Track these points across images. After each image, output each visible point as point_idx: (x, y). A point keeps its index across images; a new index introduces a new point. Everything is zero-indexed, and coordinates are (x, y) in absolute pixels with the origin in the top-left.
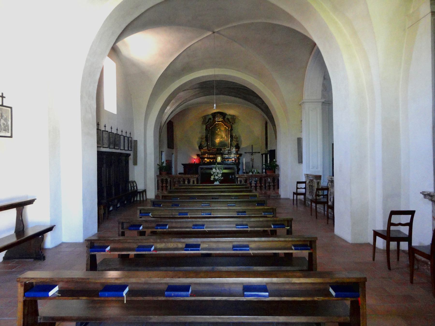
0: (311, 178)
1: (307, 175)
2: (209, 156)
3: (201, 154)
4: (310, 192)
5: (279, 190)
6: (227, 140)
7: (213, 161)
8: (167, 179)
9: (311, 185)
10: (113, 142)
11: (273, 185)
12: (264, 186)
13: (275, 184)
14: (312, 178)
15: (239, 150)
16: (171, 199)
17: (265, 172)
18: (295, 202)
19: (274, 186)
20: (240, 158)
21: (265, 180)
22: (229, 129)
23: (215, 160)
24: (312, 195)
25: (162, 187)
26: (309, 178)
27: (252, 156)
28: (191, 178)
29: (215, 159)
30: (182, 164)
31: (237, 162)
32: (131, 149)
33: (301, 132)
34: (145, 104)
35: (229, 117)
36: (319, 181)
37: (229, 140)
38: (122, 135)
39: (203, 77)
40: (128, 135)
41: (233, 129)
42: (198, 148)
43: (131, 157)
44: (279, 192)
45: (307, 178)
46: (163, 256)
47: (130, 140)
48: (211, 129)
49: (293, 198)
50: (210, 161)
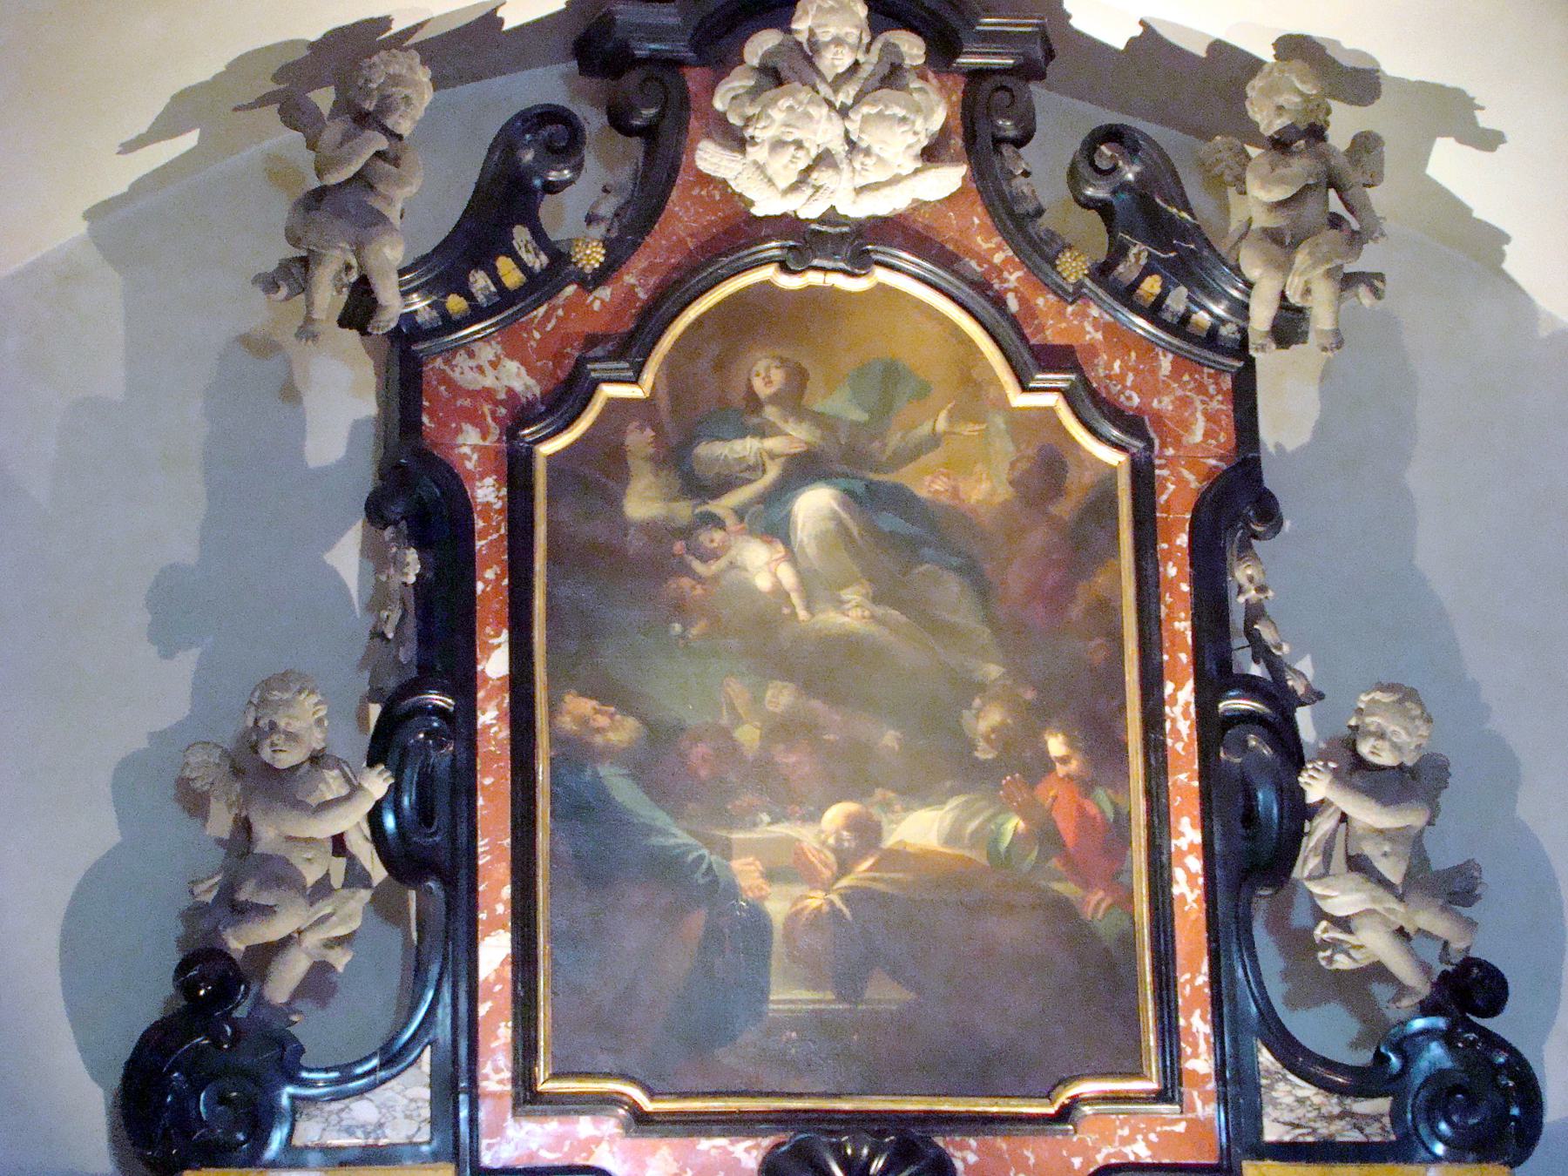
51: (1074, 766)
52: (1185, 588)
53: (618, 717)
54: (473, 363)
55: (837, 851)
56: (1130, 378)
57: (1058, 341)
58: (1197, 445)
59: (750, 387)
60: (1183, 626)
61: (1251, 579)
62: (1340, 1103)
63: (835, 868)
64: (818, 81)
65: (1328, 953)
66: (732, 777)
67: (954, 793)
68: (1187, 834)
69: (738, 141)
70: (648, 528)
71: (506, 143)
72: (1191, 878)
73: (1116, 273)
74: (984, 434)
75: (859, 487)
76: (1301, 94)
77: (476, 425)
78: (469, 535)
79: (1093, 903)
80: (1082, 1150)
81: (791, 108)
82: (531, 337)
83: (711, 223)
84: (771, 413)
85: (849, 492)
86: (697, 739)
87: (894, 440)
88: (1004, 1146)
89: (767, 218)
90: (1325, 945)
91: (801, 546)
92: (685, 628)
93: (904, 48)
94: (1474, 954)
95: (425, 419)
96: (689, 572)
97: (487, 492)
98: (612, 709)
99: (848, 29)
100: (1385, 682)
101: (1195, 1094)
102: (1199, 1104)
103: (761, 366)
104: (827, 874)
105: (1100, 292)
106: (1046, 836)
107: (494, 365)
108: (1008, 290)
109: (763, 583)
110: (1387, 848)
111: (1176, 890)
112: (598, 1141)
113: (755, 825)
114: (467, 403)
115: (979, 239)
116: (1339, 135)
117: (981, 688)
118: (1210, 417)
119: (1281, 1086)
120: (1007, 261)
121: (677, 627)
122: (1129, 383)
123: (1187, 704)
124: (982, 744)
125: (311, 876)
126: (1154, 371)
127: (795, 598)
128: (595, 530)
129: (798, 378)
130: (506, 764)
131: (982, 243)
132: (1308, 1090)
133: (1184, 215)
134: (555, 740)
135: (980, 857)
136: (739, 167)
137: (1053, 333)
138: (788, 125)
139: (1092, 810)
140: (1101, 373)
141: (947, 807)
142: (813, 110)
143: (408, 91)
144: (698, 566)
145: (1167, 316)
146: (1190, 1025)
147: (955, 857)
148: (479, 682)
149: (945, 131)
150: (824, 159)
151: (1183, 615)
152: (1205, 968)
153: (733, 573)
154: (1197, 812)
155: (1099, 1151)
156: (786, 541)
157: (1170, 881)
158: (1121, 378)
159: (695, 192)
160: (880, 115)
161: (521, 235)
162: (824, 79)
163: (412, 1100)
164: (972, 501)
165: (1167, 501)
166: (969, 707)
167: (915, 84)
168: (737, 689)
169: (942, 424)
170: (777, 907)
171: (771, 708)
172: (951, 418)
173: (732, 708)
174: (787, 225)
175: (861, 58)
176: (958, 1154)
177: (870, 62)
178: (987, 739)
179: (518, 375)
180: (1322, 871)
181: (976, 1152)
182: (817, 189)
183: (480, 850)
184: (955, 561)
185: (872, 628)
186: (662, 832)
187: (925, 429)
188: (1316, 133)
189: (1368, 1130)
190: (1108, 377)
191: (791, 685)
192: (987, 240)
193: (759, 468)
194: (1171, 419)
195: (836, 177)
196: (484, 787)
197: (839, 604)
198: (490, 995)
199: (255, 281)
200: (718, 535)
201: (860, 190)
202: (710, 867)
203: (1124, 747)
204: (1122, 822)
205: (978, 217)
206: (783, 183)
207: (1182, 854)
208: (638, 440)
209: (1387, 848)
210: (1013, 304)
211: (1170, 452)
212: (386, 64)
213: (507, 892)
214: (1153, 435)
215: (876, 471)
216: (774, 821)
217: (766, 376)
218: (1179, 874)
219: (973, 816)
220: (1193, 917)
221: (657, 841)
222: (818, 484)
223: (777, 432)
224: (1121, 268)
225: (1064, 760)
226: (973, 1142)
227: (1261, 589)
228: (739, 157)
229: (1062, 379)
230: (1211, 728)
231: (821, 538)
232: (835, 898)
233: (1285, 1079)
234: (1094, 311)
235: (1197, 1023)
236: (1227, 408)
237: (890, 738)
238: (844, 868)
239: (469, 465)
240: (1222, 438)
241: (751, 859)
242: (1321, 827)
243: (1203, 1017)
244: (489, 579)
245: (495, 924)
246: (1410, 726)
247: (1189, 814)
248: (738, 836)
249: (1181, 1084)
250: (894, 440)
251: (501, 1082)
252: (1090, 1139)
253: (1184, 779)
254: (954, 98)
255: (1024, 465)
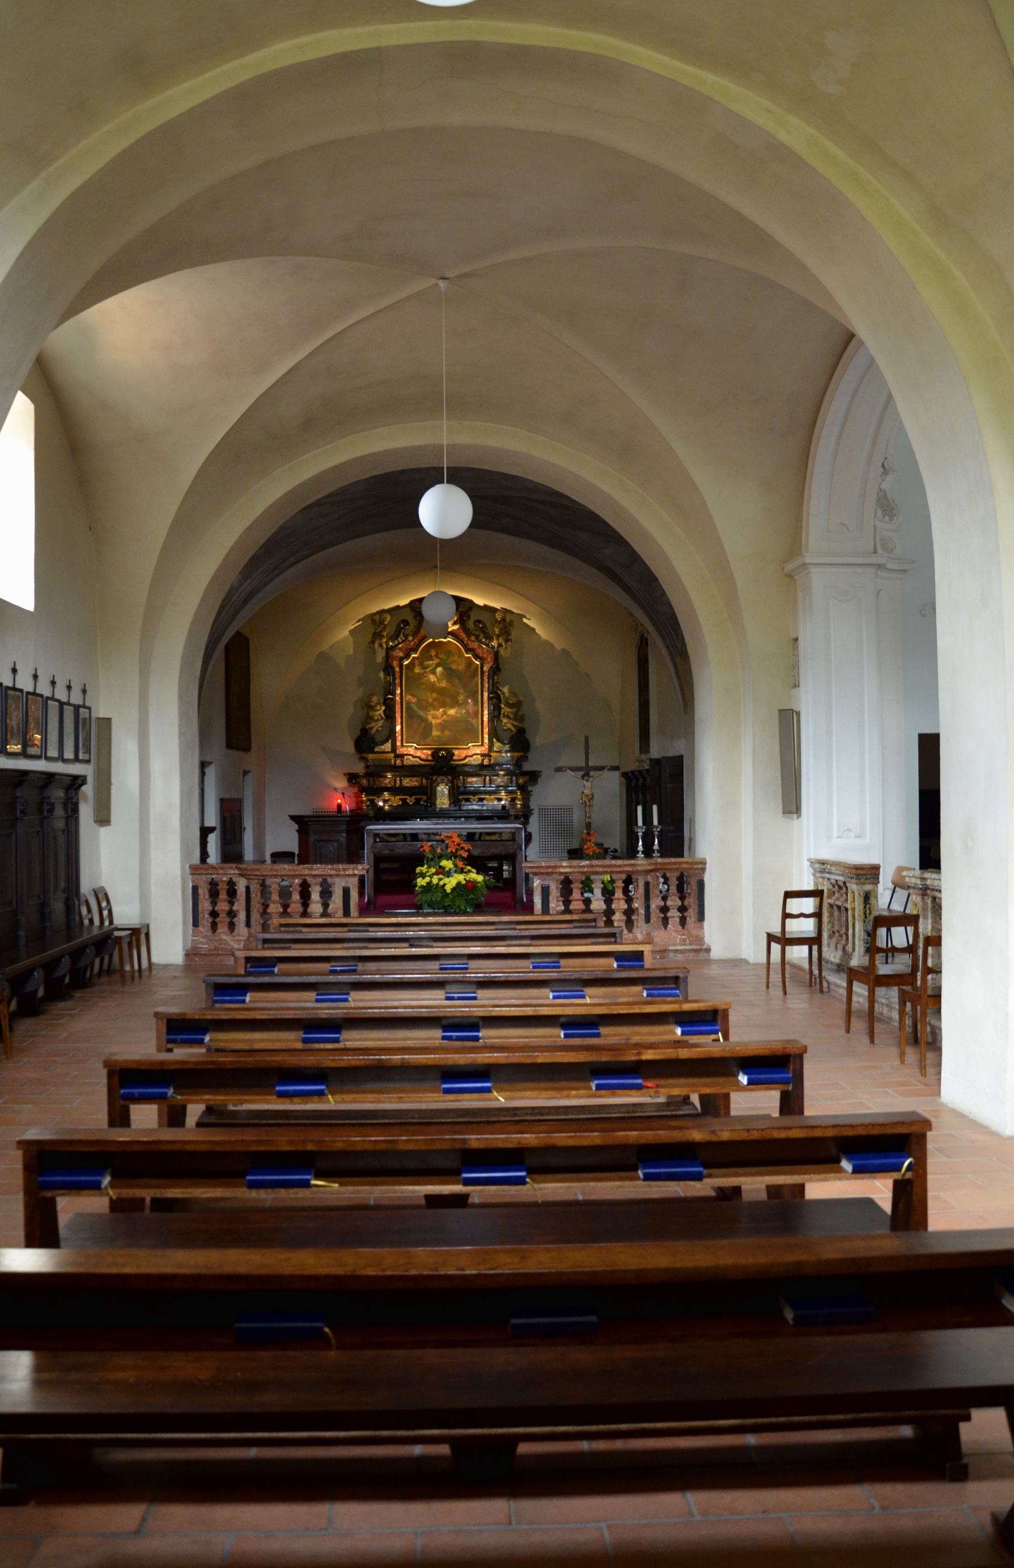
0: (839, 875)
1: (823, 863)
2: (398, 782)
3: (367, 775)
4: (834, 932)
5: (702, 928)
6: (476, 713)
7: (418, 801)
8: (234, 880)
9: (839, 903)
10: (18, 729)
11: (626, 910)
12: (642, 911)
13: (217, 908)
14: (841, 878)
15: (525, 758)
16: (830, 937)
17: (643, 852)
18: (776, 977)
19: (682, 909)
20: (530, 788)
21: (647, 885)
22: (485, 668)
23: (425, 798)
24: (840, 947)
25: (214, 914)
26: (827, 875)
27: (585, 783)
28: (337, 876)
29: (425, 794)
30: (293, 818)
31: (519, 806)
32: (86, 757)
33: (796, 685)
34: (149, 563)
35: (484, 617)
36: (868, 887)
37: (486, 712)
38: (53, 699)
39: (394, 452)
40: (76, 698)
41: (501, 666)
42: (350, 747)
43: (88, 789)
44: (703, 934)
45: (818, 875)
46: (268, 1205)
47: (81, 716)
48: (406, 665)
49: (764, 960)
50: (404, 801)
71: (399, 625)
84: (434, 658)
97: (397, 669)
106: (467, 712)
116: (508, 620)
129: (437, 653)
131: (462, 634)
134: (406, 701)
168: (429, 694)
169: (456, 658)
170: (434, 722)
193: (432, 665)
204: (478, 710)
205: (461, 631)
208: (417, 662)
217: (433, 653)
235: (486, 736)
237: (448, 700)
238: (442, 717)
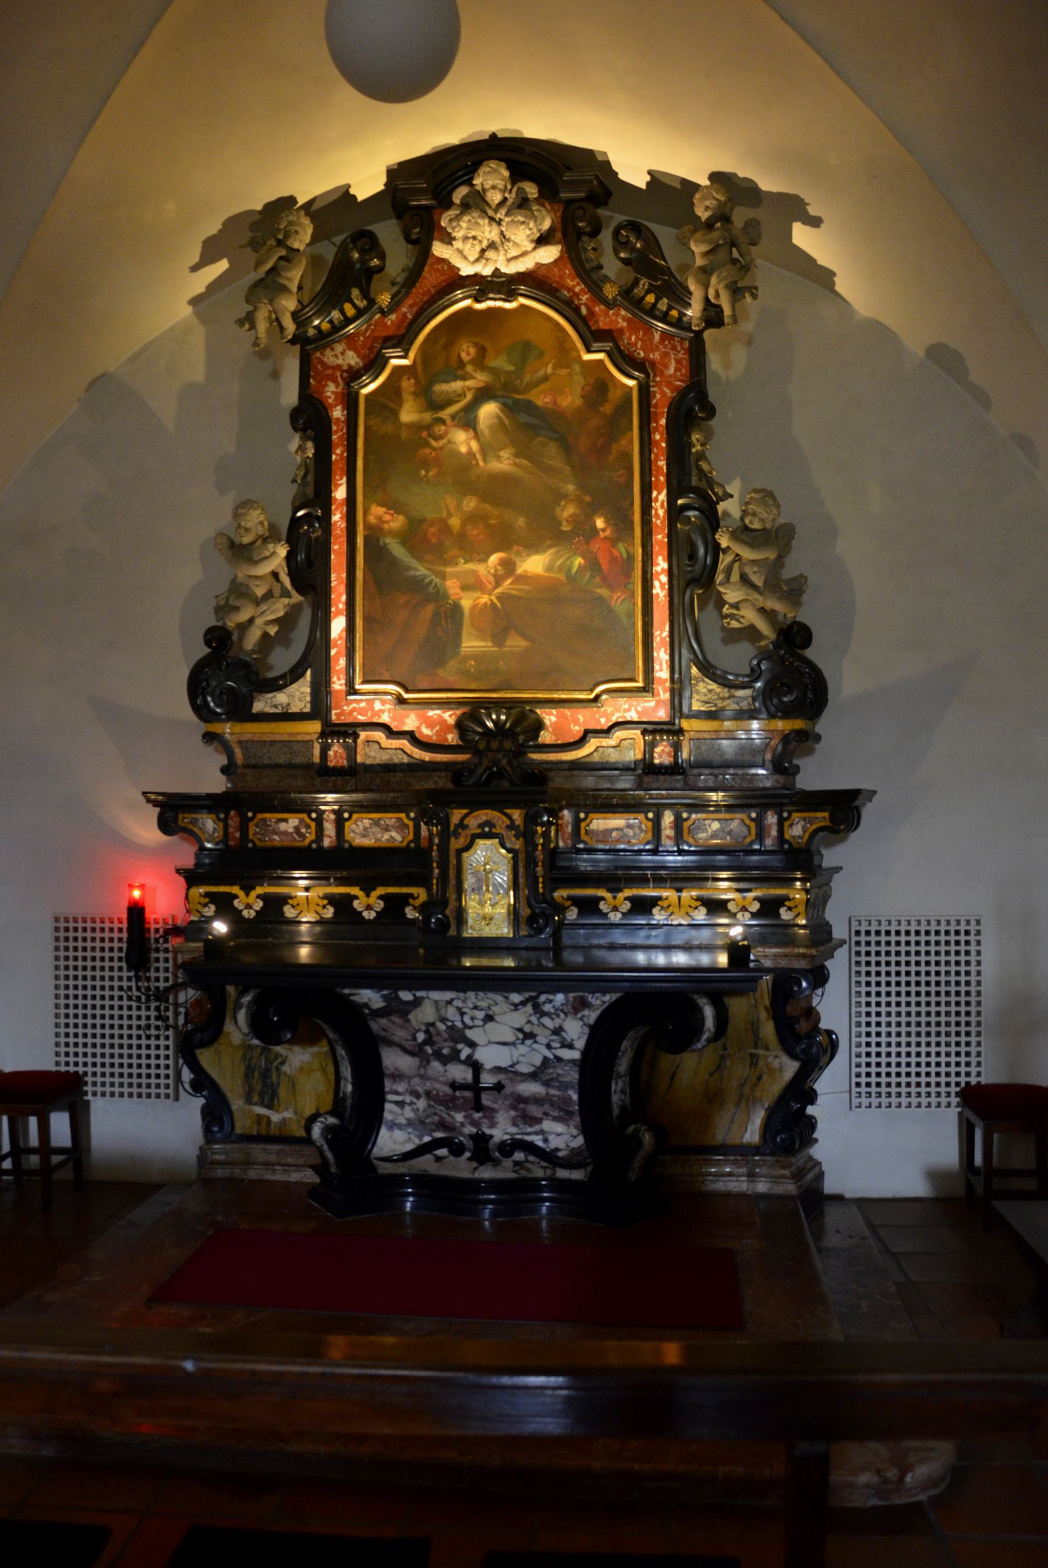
51: (608, 533)
52: (664, 445)
53: (395, 515)
54: (333, 353)
55: (495, 576)
56: (639, 344)
57: (606, 327)
58: (671, 376)
59: (459, 356)
60: (662, 463)
61: (698, 440)
62: (729, 692)
63: (494, 583)
64: (487, 208)
65: (728, 620)
66: (448, 543)
67: (550, 547)
68: (661, 564)
69: (449, 240)
70: (411, 426)
72: (662, 585)
73: (633, 293)
74: (570, 375)
75: (509, 402)
76: (716, 199)
77: (333, 382)
78: (330, 433)
79: (615, 598)
80: (606, 715)
81: (469, 220)
82: (359, 339)
83: (442, 281)
84: (469, 368)
85: (504, 404)
86: (432, 524)
87: (527, 378)
88: (569, 713)
89: (468, 276)
90: (727, 616)
91: (482, 431)
92: (427, 471)
93: (528, 190)
94: (797, 619)
95: (311, 381)
96: (428, 445)
97: (338, 413)
98: (392, 512)
99: (498, 182)
100: (759, 487)
101: (660, 688)
102: (661, 693)
103: (465, 347)
104: (490, 586)
105: (625, 303)
107: (343, 354)
108: (582, 304)
109: (463, 449)
110: (755, 569)
111: (655, 591)
112: (383, 711)
113: (457, 564)
114: (330, 372)
115: (568, 281)
117: (565, 496)
118: (678, 362)
119: (701, 684)
120: (582, 290)
121: (423, 472)
122: (639, 346)
123: (663, 501)
124: (564, 523)
125: (260, 592)
126: (652, 339)
127: (478, 456)
128: (389, 428)
129: (482, 351)
130: (344, 539)
131: (570, 283)
132: (713, 686)
133: (662, 262)
135: (562, 577)
136: (451, 252)
137: (603, 324)
138: (468, 229)
139: (616, 553)
140: (626, 342)
141: (547, 554)
142: (480, 221)
143: (297, 228)
144: (434, 443)
145: (658, 313)
146: (659, 656)
147: (550, 578)
148: (333, 501)
149: (551, 230)
150: (492, 246)
151: (662, 458)
152: (667, 628)
153: (450, 446)
154: (666, 553)
155: (613, 715)
156: (475, 429)
157: (652, 586)
158: (635, 344)
159: (436, 267)
160: (512, 221)
161: (355, 293)
162: (490, 207)
163: (302, 693)
164: (563, 407)
165: (656, 403)
166: (559, 505)
167: (535, 207)
168: (450, 502)
169: (549, 370)
170: (466, 603)
171: (465, 509)
172: (554, 367)
173: (448, 509)
174: (476, 278)
175: (507, 195)
176: (547, 717)
177: (511, 197)
178: (567, 520)
179: (353, 358)
180: (725, 580)
181: (556, 716)
182: (487, 260)
183: (332, 579)
184: (556, 435)
185: (514, 469)
186: (416, 569)
187: (542, 372)
188: (726, 219)
189: (741, 704)
190: (629, 344)
191: (474, 498)
192: (573, 281)
193: (463, 395)
194: (659, 363)
195: (496, 254)
196: (335, 550)
197: (499, 458)
198: (336, 646)
199: (236, 323)
200: (443, 428)
201: (509, 260)
202: (436, 584)
203: (632, 522)
204: (631, 558)
206: (472, 259)
207: (658, 574)
209: (755, 569)
210: (584, 311)
211: (658, 379)
212: (287, 216)
213: (344, 598)
214: (650, 371)
215: (518, 393)
216: (466, 562)
218: (656, 583)
219: (560, 557)
220: (662, 604)
221: (411, 573)
222: (491, 401)
223: (473, 378)
224: (635, 291)
225: (604, 530)
226: (554, 712)
227: (703, 445)
228: (450, 247)
229: (608, 346)
230: (674, 513)
231: (491, 427)
232: (493, 598)
233: (703, 680)
234: (623, 312)
235: (662, 655)
236: (686, 357)
237: (521, 522)
239: (330, 401)
240: (683, 371)
241: (455, 580)
242: (725, 560)
243: (665, 652)
244: (338, 454)
245: (338, 613)
246: (768, 510)
247: (663, 555)
248: (449, 570)
249: (653, 684)
250: (527, 378)
251: (341, 685)
252: (609, 710)
253: (660, 538)
254: (558, 214)
255: (588, 388)
